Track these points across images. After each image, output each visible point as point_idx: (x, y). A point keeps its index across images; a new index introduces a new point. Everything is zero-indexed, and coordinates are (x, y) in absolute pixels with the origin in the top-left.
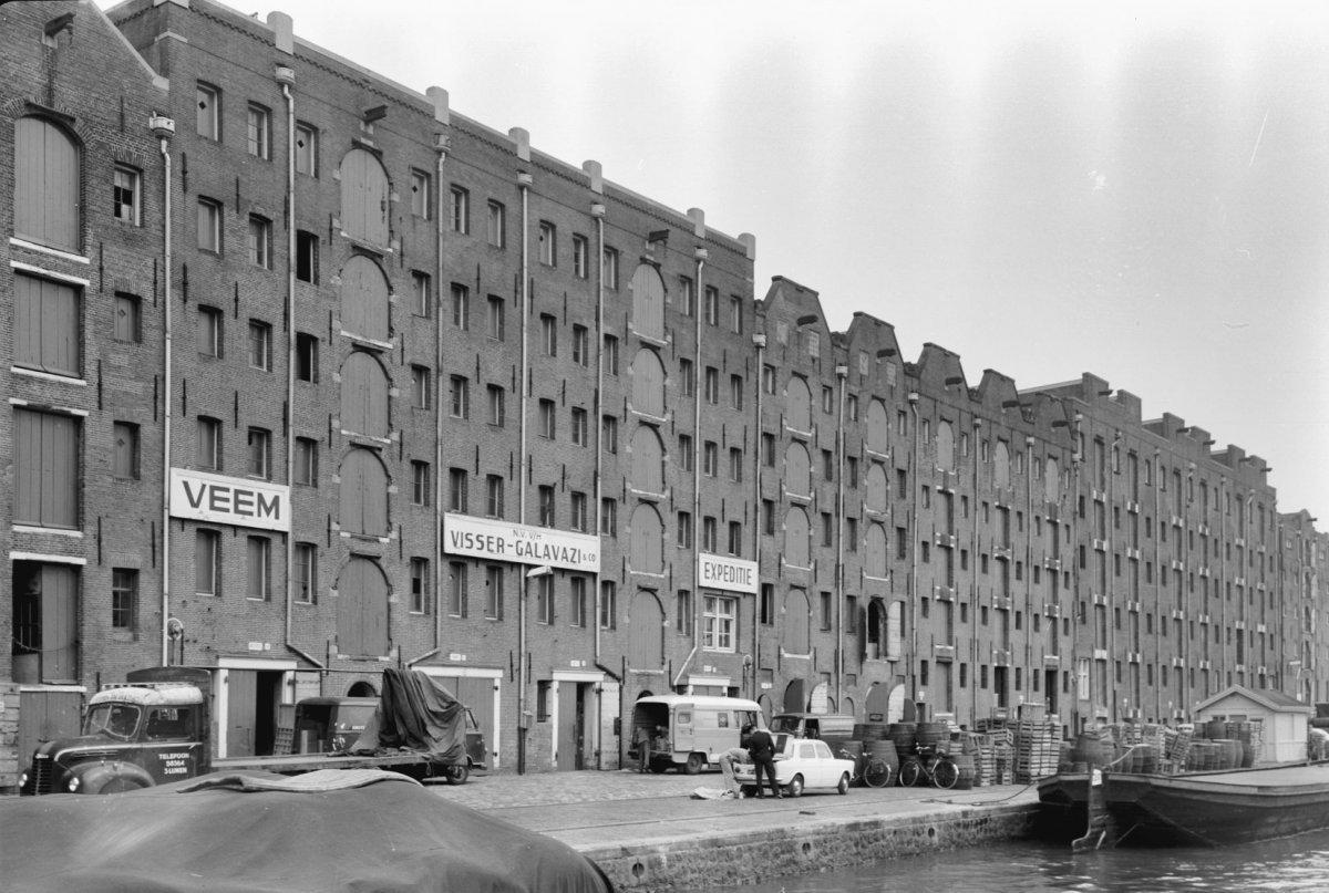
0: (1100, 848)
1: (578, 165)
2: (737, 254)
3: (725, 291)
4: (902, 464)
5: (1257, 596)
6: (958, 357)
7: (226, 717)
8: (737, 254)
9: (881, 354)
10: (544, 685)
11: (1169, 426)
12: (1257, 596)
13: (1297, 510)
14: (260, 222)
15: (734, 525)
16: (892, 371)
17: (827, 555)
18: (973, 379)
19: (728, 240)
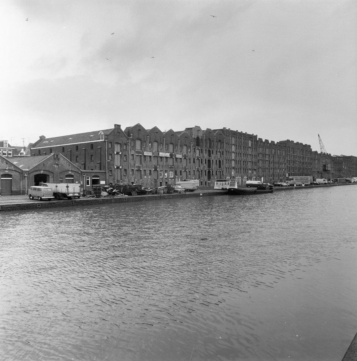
0: (73, 177)
1: (245, 133)
2: (256, 136)
3: (255, 141)
4: (269, 154)
5: (292, 161)
6: (310, 146)
7: (253, 183)
8: (256, 136)
9: (261, 142)
10: (243, 178)
11: (298, 143)
12: (292, 161)
13: (315, 151)
14: (229, 144)
15: (256, 162)
16: (268, 144)
17: (263, 164)
18: (270, 142)
19: (235, 131)
